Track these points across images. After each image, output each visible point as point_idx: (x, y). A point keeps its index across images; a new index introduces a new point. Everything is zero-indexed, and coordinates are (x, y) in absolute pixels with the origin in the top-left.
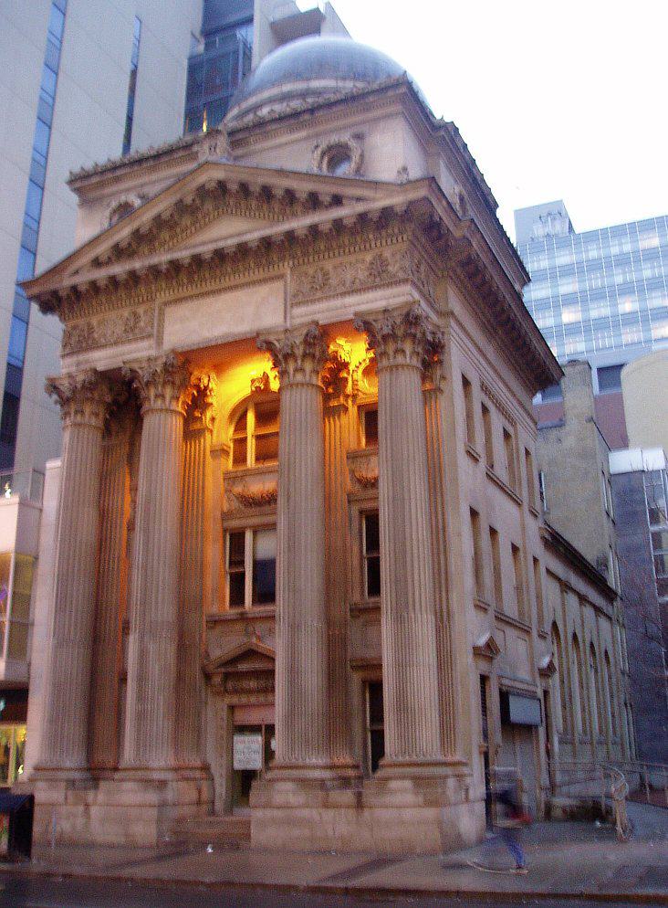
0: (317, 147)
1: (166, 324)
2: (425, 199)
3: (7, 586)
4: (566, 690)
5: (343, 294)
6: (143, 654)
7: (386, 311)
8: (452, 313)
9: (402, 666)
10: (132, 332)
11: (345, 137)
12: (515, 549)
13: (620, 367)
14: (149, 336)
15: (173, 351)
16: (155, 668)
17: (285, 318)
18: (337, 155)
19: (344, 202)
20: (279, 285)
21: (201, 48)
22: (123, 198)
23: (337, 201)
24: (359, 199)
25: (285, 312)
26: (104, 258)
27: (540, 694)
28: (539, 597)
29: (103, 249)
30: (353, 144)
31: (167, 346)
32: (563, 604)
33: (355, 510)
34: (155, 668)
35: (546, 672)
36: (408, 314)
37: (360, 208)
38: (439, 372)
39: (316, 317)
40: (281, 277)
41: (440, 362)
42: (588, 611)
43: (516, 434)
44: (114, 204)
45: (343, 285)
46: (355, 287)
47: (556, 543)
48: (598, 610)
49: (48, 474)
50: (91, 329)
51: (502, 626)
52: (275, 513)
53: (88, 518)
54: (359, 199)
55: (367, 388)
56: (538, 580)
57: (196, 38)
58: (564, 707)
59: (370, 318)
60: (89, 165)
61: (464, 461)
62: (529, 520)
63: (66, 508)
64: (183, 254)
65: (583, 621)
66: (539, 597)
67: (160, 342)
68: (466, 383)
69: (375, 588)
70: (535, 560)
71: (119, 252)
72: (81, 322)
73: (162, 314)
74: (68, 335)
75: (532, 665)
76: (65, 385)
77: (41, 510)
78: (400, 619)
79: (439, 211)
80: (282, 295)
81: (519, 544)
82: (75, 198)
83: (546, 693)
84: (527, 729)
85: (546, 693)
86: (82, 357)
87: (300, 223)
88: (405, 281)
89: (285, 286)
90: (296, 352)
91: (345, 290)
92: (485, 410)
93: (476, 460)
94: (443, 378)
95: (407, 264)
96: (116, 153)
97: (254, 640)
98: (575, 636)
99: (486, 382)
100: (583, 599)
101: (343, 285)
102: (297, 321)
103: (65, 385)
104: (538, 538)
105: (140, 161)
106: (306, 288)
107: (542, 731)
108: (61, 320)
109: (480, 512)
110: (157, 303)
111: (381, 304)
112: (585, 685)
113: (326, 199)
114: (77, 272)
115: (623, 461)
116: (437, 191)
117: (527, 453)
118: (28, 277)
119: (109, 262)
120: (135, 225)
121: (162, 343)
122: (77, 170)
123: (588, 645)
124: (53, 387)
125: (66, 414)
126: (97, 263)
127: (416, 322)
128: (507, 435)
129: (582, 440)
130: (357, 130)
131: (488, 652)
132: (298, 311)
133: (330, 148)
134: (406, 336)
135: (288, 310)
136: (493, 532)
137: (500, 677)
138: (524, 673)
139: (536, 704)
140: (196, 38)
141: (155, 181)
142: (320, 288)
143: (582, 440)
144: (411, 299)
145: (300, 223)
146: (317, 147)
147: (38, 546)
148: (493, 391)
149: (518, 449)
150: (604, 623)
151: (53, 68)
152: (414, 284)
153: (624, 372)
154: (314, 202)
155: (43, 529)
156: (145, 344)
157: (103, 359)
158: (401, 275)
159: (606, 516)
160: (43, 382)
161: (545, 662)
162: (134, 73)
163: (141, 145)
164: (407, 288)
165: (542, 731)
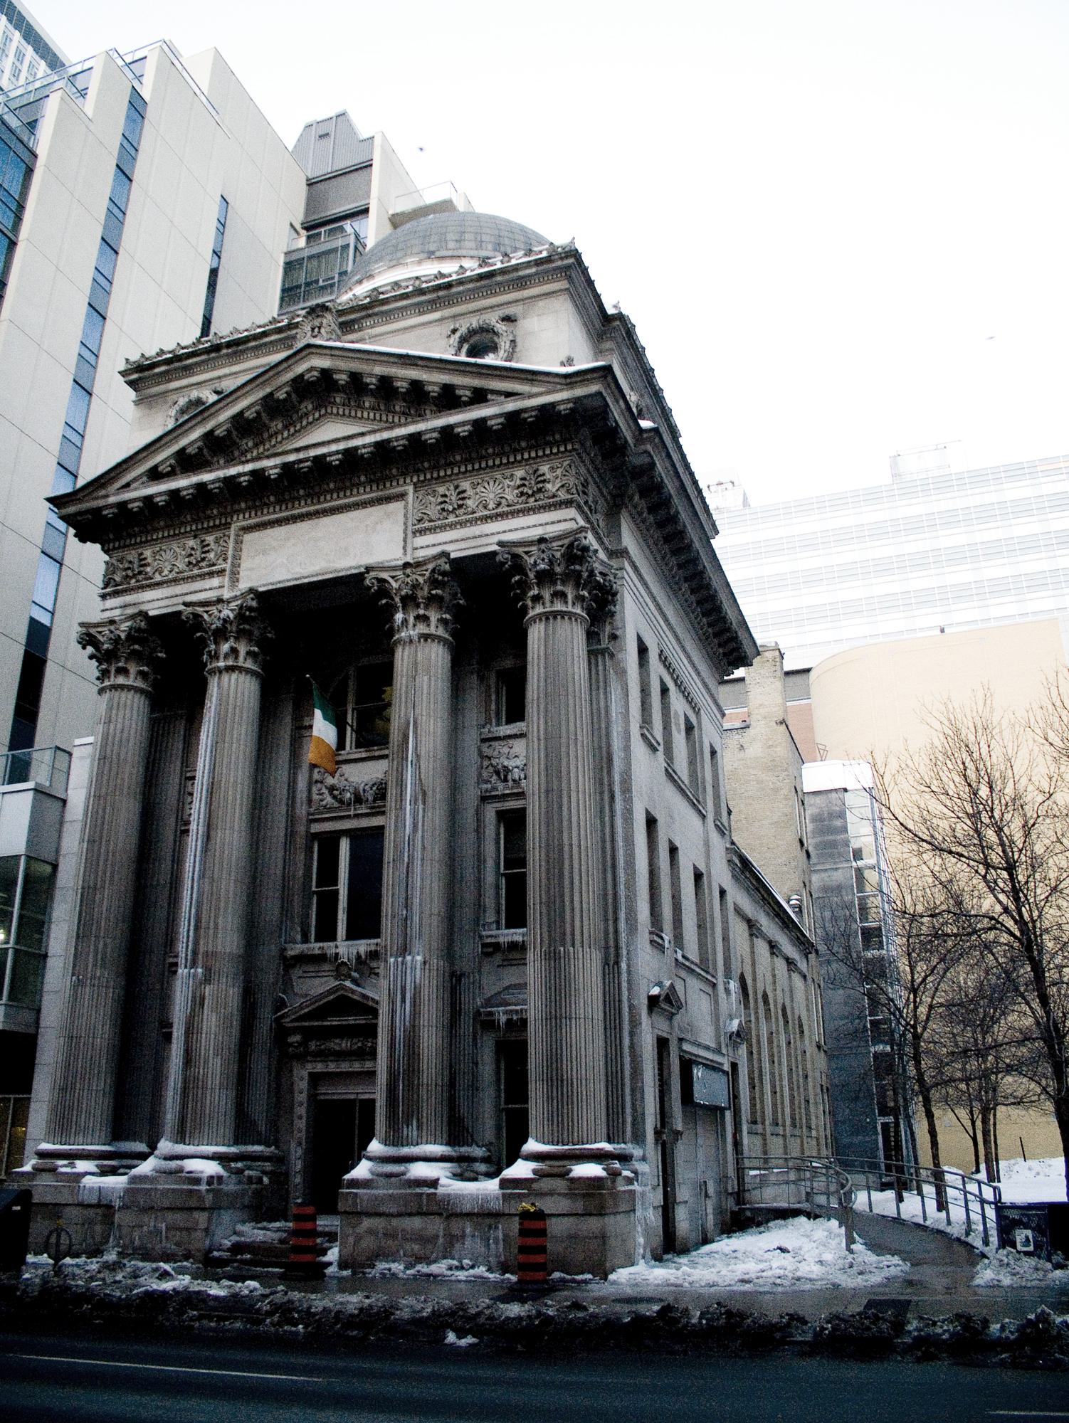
0: (454, 331)
1: (244, 554)
2: (599, 394)
3: (13, 907)
4: (756, 1065)
5: (485, 519)
6: (198, 1002)
7: (542, 540)
8: (627, 553)
9: (557, 1017)
10: (200, 568)
11: (492, 319)
12: (698, 876)
13: (808, 671)
14: (221, 572)
15: (251, 590)
16: (211, 1022)
17: (404, 548)
18: (480, 341)
19: (489, 397)
20: (397, 506)
21: (302, 242)
22: (194, 394)
23: (480, 397)
24: (509, 395)
25: (405, 540)
26: (164, 468)
27: (727, 1067)
28: (726, 939)
29: (162, 456)
30: (501, 327)
31: (244, 585)
32: (753, 953)
33: (490, 812)
34: (211, 1022)
35: (740, 1036)
36: (571, 545)
37: (511, 406)
38: (608, 629)
39: (448, 548)
40: (402, 496)
41: (612, 614)
42: (780, 964)
43: (699, 723)
44: (182, 401)
45: (485, 507)
46: (500, 510)
47: (744, 869)
48: (790, 962)
49: (76, 753)
50: (143, 563)
51: (683, 974)
52: (383, 813)
53: (127, 812)
54: (509, 395)
55: (247, 1173)
56: (725, 921)
57: (295, 230)
58: (753, 1087)
59: (520, 550)
60: (151, 352)
61: (638, 747)
62: (714, 835)
63: (98, 797)
64: (271, 465)
65: (774, 976)
66: (726, 939)
67: (235, 579)
68: (643, 650)
69: (517, 916)
70: (723, 893)
71: (186, 462)
72: (132, 555)
73: (238, 542)
74: (110, 570)
75: (717, 1028)
76: (104, 636)
77: (64, 802)
78: (553, 957)
79: (616, 414)
80: (401, 519)
81: (702, 868)
82: (131, 394)
83: (734, 1066)
84: (715, 1111)
85: (734, 1066)
86: (129, 598)
87: (430, 425)
88: (568, 503)
89: (405, 508)
90: (419, 593)
91: (486, 513)
92: (664, 691)
93: (654, 750)
94: (614, 637)
95: (572, 481)
96: (185, 334)
97: (348, 984)
98: (765, 996)
99: (667, 652)
100: (773, 947)
101: (485, 507)
102: (421, 554)
103: (104, 636)
104: (725, 862)
105: (216, 348)
106: (433, 511)
107: (728, 1114)
108: (103, 549)
109: (658, 816)
110: (232, 529)
111: (536, 533)
112: (776, 1059)
113: (465, 394)
114: (127, 485)
115: (815, 777)
116: (613, 386)
117: (713, 753)
118: (65, 487)
119: (171, 474)
120: (209, 426)
121: (238, 580)
122: (135, 357)
123: (780, 1006)
124: (88, 639)
125: (104, 674)
126: (155, 475)
127: (583, 557)
128: (689, 728)
129: (770, 747)
130: (510, 311)
131: (664, 1004)
132: (421, 541)
133: (472, 332)
134: (566, 578)
135: (409, 540)
136: (673, 850)
137: (681, 1040)
138: (707, 1037)
139: (724, 1079)
140: (295, 230)
141: (234, 374)
142: (455, 514)
143: (770, 747)
144: (574, 526)
145: (430, 425)
146: (454, 331)
147: (58, 851)
148: (675, 665)
149: (702, 748)
150: (796, 978)
151: (110, 245)
152: (579, 507)
153: (812, 673)
154: (449, 399)
155: (67, 827)
156: (215, 582)
157: (156, 601)
158: (563, 495)
159: (798, 845)
160: (75, 631)
161: (735, 1025)
162: (214, 273)
163: (223, 328)
164: (572, 512)
165: (728, 1114)
